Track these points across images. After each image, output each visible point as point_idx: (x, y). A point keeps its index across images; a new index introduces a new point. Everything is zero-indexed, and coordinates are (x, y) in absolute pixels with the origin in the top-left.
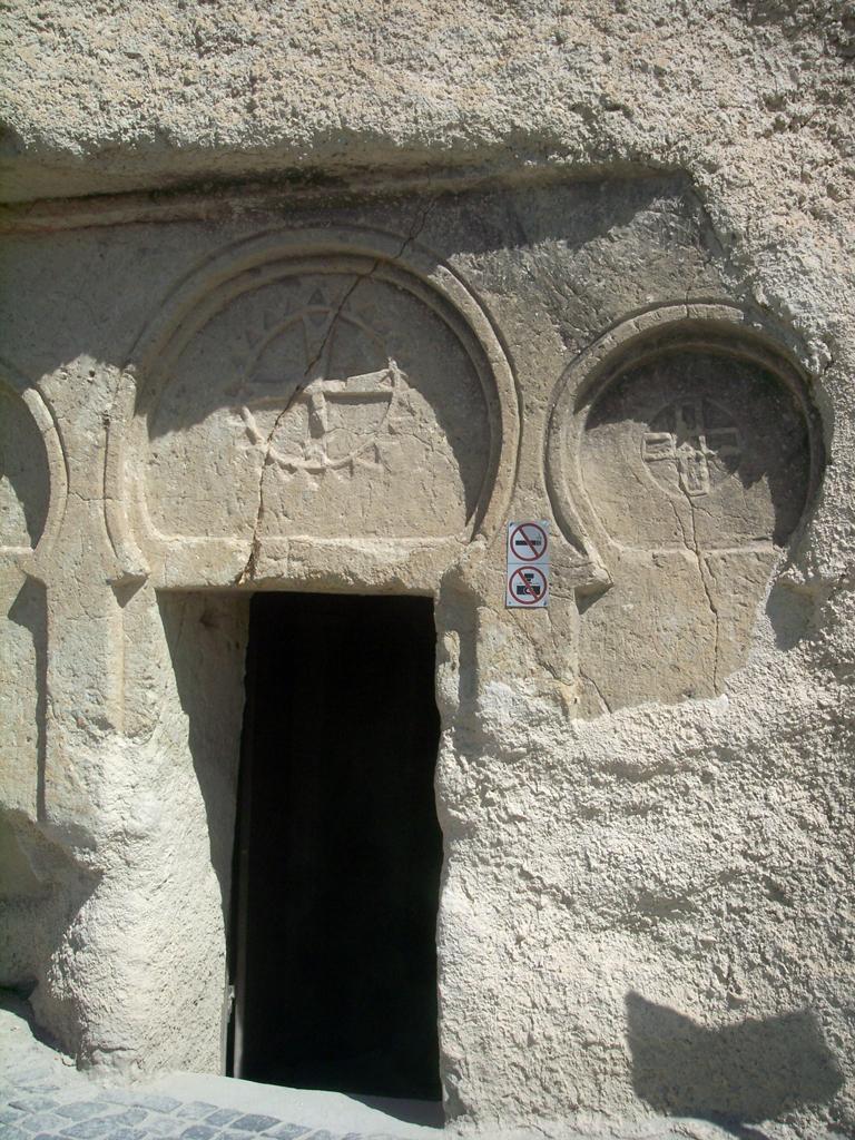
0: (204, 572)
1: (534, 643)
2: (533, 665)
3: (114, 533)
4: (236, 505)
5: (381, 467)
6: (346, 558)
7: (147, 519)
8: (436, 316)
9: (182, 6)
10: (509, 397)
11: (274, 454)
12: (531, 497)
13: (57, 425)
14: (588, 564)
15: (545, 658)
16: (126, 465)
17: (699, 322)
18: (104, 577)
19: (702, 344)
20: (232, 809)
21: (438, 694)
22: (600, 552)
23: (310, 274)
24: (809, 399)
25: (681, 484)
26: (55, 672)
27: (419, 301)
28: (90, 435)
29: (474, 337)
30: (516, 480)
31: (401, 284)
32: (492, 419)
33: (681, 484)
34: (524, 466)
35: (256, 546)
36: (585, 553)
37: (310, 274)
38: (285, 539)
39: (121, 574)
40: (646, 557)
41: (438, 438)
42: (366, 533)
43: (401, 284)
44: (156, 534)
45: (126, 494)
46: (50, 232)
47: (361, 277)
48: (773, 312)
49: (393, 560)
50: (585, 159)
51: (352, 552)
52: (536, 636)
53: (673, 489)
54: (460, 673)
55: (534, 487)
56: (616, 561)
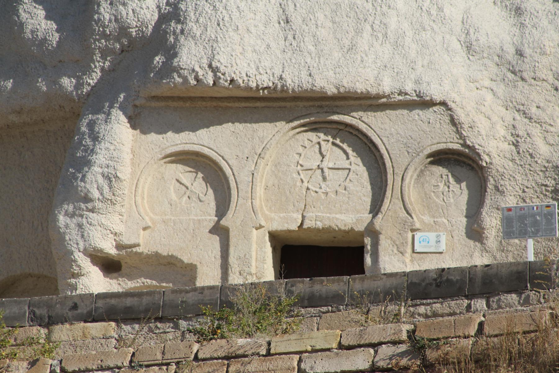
0: (286, 225)
1: (397, 245)
2: (396, 251)
3: (255, 211)
4: (296, 204)
5: (347, 192)
6: (335, 220)
7: (264, 207)
8: (366, 144)
9: (111, 4)
10: (390, 171)
11: (310, 187)
12: (397, 201)
13: (233, 174)
14: (413, 222)
15: (400, 250)
16: (258, 188)
17: (449, 149)
18: (252, 225)
19: (451, 156)
20: (322, 245)
21: (365, 263)
22: (417, 219)
23: (323, 128)
24: (482, 173)
25: (443, 200)
26: (232, 258)
27: (360, 139)
28: (246, 178)
29: (379, 151)
30: (392, 196)
31: (354, 132)
32: (384, 178)
33: (443, 200)
34: (394, 192)
35: (303, 217)
36: (413, 218)
37: (323, 128)
38: (314, 214)
39: (258, 225)
40: (432, 220)
41: (365, 183)
42: (341, 213)
43: (354, 132)
44: (267, 212)
45: (258, 199)
46: (231, 108)
47: (340, 130)
48: (472, 148)
49: (351, 222)
50: (416, 98)
51: (337, 219)
52: (397, 243)
53: (441, 201)
54: (371, 257)
55: (398, 198)
56: (422, 222)
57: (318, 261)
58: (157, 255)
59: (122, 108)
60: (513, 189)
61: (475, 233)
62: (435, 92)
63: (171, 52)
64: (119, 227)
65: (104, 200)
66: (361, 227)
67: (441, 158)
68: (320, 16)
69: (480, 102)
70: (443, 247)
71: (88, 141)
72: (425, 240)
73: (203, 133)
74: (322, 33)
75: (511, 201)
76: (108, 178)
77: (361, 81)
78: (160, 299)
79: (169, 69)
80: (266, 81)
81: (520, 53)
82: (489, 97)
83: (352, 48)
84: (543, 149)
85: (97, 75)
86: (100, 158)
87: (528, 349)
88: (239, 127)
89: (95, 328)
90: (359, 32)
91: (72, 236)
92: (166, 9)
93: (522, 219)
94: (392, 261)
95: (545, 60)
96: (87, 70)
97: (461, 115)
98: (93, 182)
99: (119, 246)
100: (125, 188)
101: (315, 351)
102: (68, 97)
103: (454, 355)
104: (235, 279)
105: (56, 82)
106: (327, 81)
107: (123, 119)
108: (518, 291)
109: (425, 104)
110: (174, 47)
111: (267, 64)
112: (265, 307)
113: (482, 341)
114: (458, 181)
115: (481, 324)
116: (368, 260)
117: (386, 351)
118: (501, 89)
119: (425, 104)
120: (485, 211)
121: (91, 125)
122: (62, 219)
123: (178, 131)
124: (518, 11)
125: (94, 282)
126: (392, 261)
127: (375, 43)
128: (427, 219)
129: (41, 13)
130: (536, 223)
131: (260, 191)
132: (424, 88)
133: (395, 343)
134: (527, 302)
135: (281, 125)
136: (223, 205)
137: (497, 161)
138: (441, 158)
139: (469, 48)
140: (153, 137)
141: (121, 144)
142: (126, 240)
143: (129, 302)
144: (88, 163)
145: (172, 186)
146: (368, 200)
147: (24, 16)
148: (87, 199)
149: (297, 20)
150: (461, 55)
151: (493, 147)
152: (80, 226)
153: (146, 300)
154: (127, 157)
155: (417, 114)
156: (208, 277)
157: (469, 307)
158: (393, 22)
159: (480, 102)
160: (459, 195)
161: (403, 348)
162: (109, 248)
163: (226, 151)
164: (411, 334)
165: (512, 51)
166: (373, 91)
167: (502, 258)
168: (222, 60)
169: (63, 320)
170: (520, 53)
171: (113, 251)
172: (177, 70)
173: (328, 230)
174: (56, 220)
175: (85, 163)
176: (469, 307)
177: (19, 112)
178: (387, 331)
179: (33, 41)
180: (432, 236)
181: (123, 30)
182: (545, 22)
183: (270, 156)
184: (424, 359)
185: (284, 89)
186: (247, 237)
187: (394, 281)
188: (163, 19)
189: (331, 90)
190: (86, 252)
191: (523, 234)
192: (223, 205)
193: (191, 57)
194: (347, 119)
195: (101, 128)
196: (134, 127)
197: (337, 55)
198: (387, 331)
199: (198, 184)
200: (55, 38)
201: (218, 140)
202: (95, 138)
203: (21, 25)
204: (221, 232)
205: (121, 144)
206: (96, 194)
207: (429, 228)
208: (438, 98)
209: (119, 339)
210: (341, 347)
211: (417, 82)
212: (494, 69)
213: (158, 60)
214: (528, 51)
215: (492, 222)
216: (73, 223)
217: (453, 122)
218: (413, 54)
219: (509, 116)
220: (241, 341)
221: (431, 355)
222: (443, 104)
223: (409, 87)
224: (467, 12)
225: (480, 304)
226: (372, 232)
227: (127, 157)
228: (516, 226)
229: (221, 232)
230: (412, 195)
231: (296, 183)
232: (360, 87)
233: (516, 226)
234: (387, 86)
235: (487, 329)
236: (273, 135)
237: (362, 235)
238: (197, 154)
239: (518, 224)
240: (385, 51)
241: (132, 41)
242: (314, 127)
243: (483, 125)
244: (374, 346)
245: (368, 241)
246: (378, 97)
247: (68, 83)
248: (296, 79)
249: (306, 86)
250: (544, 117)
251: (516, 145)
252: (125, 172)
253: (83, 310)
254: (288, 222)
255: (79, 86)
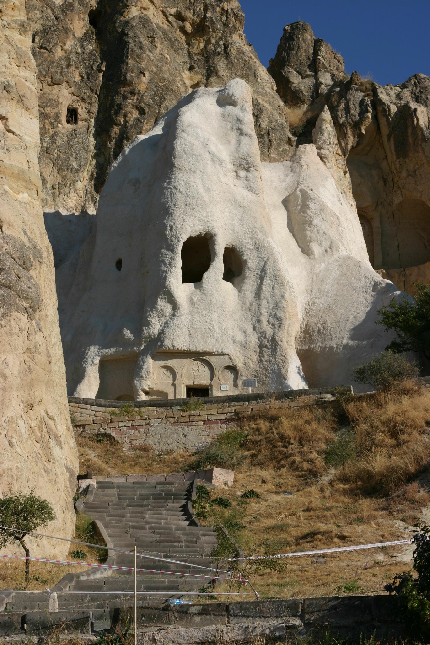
48: (235, 365)
57: (198, 392)
58: (158, 391)
59: (150, 355)
60: (245, 375)
61: (236, 385)
62: (226, 352)
63: (162, 342)
64: (149, 384)
65: (146, 377)
66: (208, 384)
67: (227, 367)
68: (198, 333)
69: (237, 354)
70: (228, 389)
71: (142, 363)
72: (223, 387)
73: (169, 361)
74: (199, 337)
75: (244, 378)
76: (147, 372)
77: (208, 348)
78: (161, 402)
79: (162, 346)
80: (185, 349)
81: (246, 343)
82: (239, 353)
83: (206, 341)
84: (252, 366)
85: (143, 347)
86: (145, 367)
87: (264, 414)
88: (178, 359)
89: (151, 408)
90: (207, 337)
91: (138, 386)
92: (160, 331)
93: (248, 382)
94: (216, 393)
95: (252, 344)
96: (141, 346)
97: (232, 357)
98: (143, 373)
99: (149, 388)
100: (151, 375)
101: (211, 414)
102: (136, 352)
103: (246, 415)
104: (178, 397)
105: (132, 349)
106: (200, 349)
107: (150, 358)
108: (256, 400)
109: (223, 354)
110: (163, 340)
111: (185, 344)
112: (182, 403)
113: (253, 412)
114: (231, 373)
115: (252, 408)
116: (210, 392)
117: (229, 414)
118: (241, 351)
119: (223, 354)
120: (238, 380)
121: (142, 359)
122: (136, 382)
123: (163, 361)
124: (245, 333)
125: (143, 397)
126: (216, 393)
127: (314, 327)
128: (224, 382)
129: (129, 332)
130: (251, 383)
131: (183, 375)
132: (223, 351)
133: (231, 413)
134: (258, 403)
135: (188, 359)
136: (174, 378)
137: (241, 368)
138: (227, 367)
139: (234, 341)
140: (157, 362)
141: (150, 364)
142: (151, 387)
143: (159, 402)
144: (142, 368)
145: (162, 374)
146: (210, 377)
147: (125, 333)
148: (142, 377)
149: (192, 334)
150: (232, 343)
151: (240, 365)
152: (140, 383)
153: (163, 402)
154: (152, 367)
155: (222, 357)
156: (171, 397)
157: (244, 404)
158: (216, 335)
159: (237, 354)
160: (231, 377)
161: (233, 414)
162: (147, 388)
163: (175, 366)
164: (235, 410)
165: (244, 342)
166: (211, 351)
167: (244, 393)
168: (175, 344)
169: (143, 406)
170: (246, 343)
171: (148, 390)
172: (164, 346)
173: (200, 385)
174: (134, 382)
175: (141, 368)
176: (244, 404)
177: (123, 356)
178: (229, 410)
179: (127, 339)
180: (225, 386)
181: (150, 336)
182: (251, 335)
183: (186, 367)
184: (238, 416)
185: (190, 351)
186: (180, 386)
187: (224, 398)
188: (160, 334)
189: (201, 351)
190: (142, 390)
191: (248, 386)
192: (174, 378)
193: (167, 343)
194: (204, 358)
195: (145, 360)
196: (153, 359)
197: (202, 342)
198: (229, 410)
199: (168, 373)
200: (132, 338)
201: (172, 363)
202: (144, 362)
203: (124, 335)
204: (174, 385)
205: (150, 364)
206: (144, 376)
207: (225, 384)
208: (226, 353)
209: (157, 411)
210: (218, 413)
211: (222, 349)
212: (239, 346)
213: (159, 343)
214: (248, 342)
215: (240, 383)
216: (138, 383)
217: (230, 359)
218: (220, 342)
219: (243, 357)
220: (193, 412)
221: (240, 416)
222: (228, 354)
223: (220, 350)
224: (233, 333)
225: (247, 403)
226: (211, 385)
227: (152, 367)
228: (247, 384)
229: (174, 385)
230: (220, 376)
231: (193, 373)
232: (208, 350)
233: (247, 384)
234: (214, 350)
235: (254, 410)
236: (186, 361)
237: (208, 386)
238: (168, 366)
239: (246, 384)
240: (214, 342)
241: (152, 339)
242: (196, 360)
243: (237, 360)
244: (226, 413)
245: (210, 387)
246: (212, 353)
247: (136, 349)
248: (193, 348)
249: (195, 350)
250: (252, 358)
251: (245, 364)
252: (151, 370)
253: (147, 404)
254: (190, 382)
255: (138, 350)
